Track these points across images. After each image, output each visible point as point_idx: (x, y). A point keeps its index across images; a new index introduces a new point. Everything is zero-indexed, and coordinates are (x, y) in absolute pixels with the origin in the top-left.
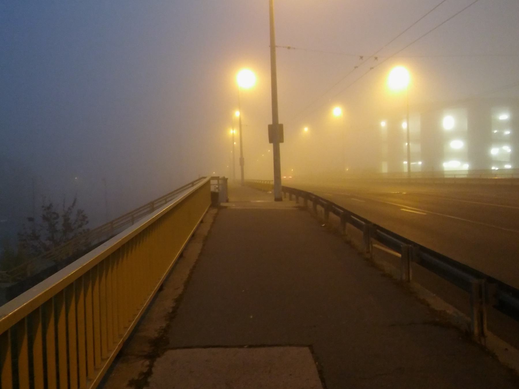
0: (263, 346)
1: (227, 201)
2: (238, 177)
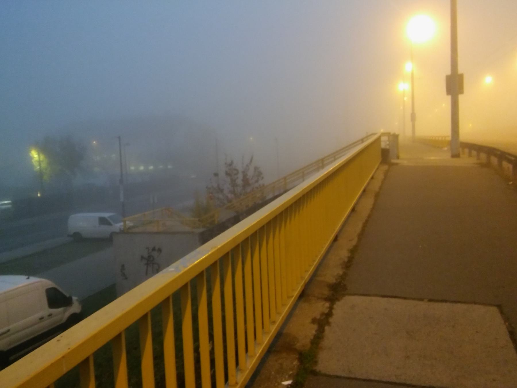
0: (446, 301)
1: (398, 158)
2: (409, 132)
